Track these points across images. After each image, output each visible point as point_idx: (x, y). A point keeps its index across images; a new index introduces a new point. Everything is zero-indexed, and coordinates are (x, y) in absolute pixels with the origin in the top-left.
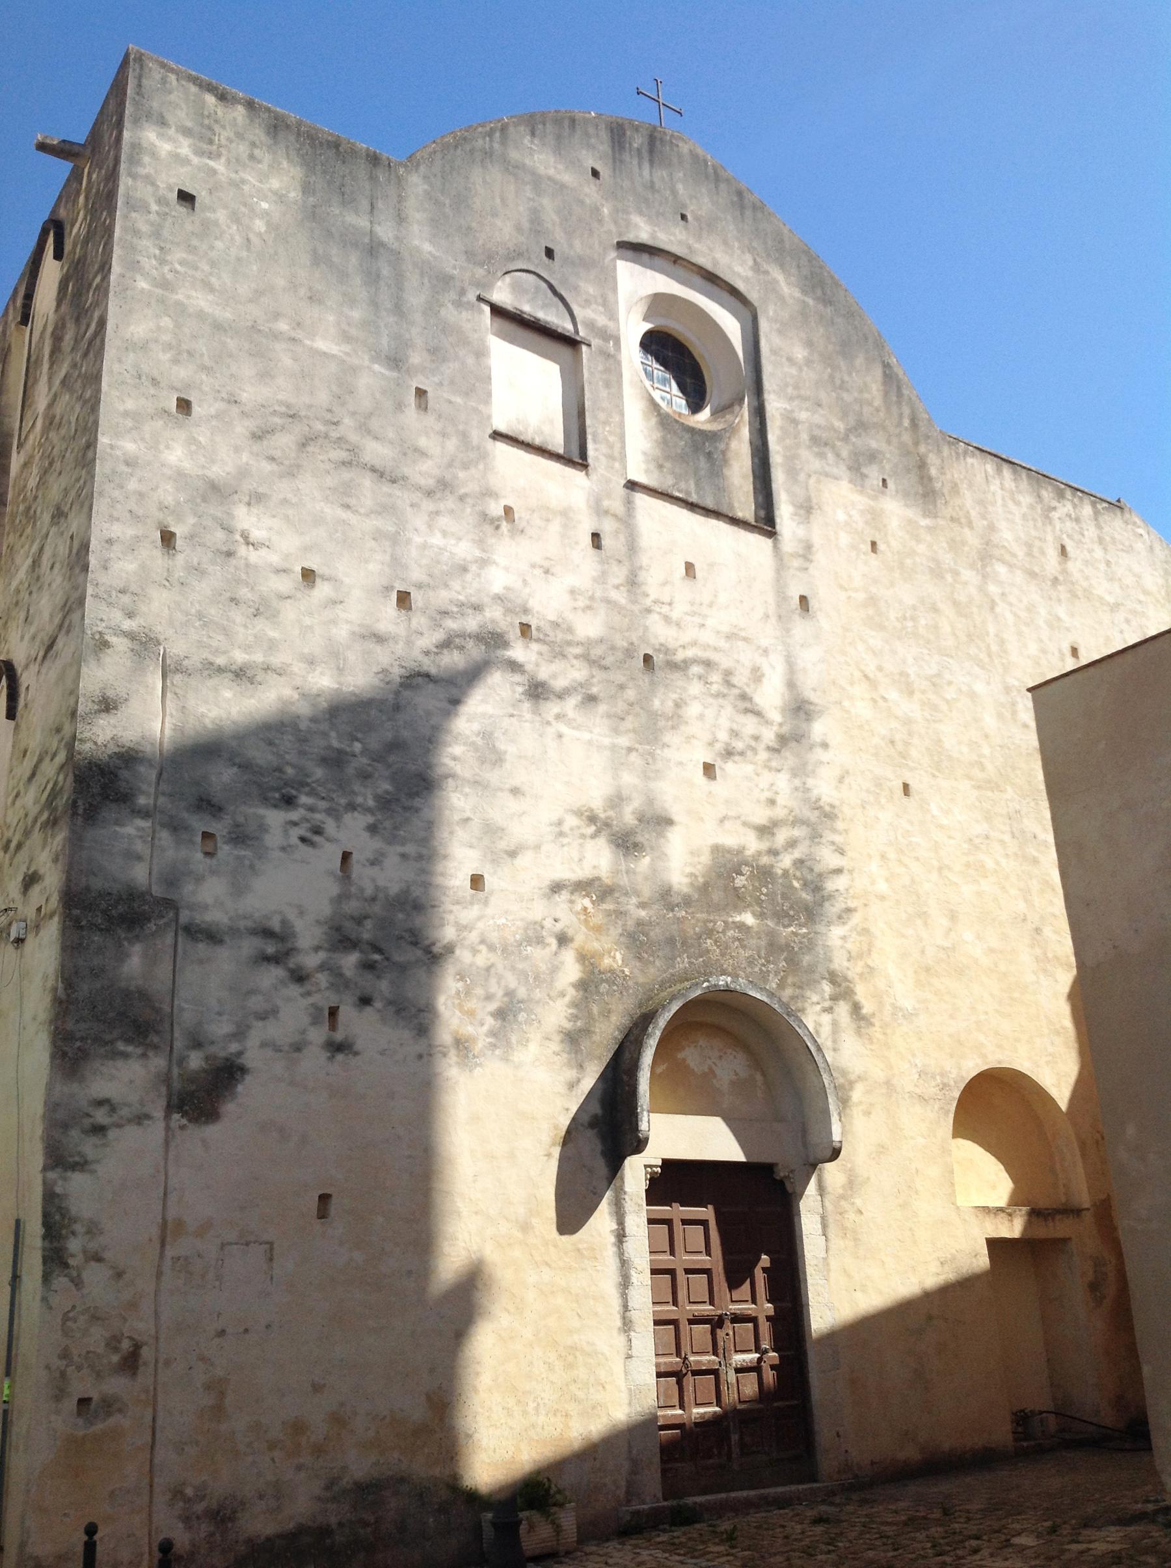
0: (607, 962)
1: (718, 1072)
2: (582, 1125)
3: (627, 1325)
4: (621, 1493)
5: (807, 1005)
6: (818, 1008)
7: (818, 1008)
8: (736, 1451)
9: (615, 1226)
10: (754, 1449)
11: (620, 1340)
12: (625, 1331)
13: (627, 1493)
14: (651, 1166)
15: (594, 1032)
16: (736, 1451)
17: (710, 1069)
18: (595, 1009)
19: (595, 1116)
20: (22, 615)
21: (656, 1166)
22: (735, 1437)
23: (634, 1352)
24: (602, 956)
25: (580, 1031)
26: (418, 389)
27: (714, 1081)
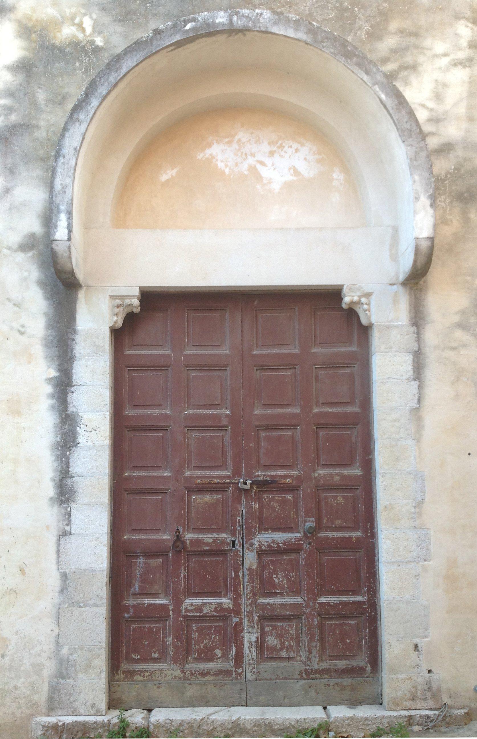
0: (67, 32)
1: (265, 172)
2: (9, 248)
3: (65, 492)
4: (42, 697)
5: (421, 59)
6: (445, 61)
7: (445, 61)
8: (250, 653)
9: (53, 373)
10: (284, 654)
11: (51, 515)
12: (61, 503)
13: (51, 699)
14: (122, 297)
15: (37, 127)
16: (250, 653)
17: (252, 169)
18: (41, 96)
19: (32, 235)
20: (309, 41)
21: (133, 297)
22: (250, 637)
23: (74, 528)
24: (58, 24)
25: (14, 127)
26: (428, 673)
27: (259, 187)
